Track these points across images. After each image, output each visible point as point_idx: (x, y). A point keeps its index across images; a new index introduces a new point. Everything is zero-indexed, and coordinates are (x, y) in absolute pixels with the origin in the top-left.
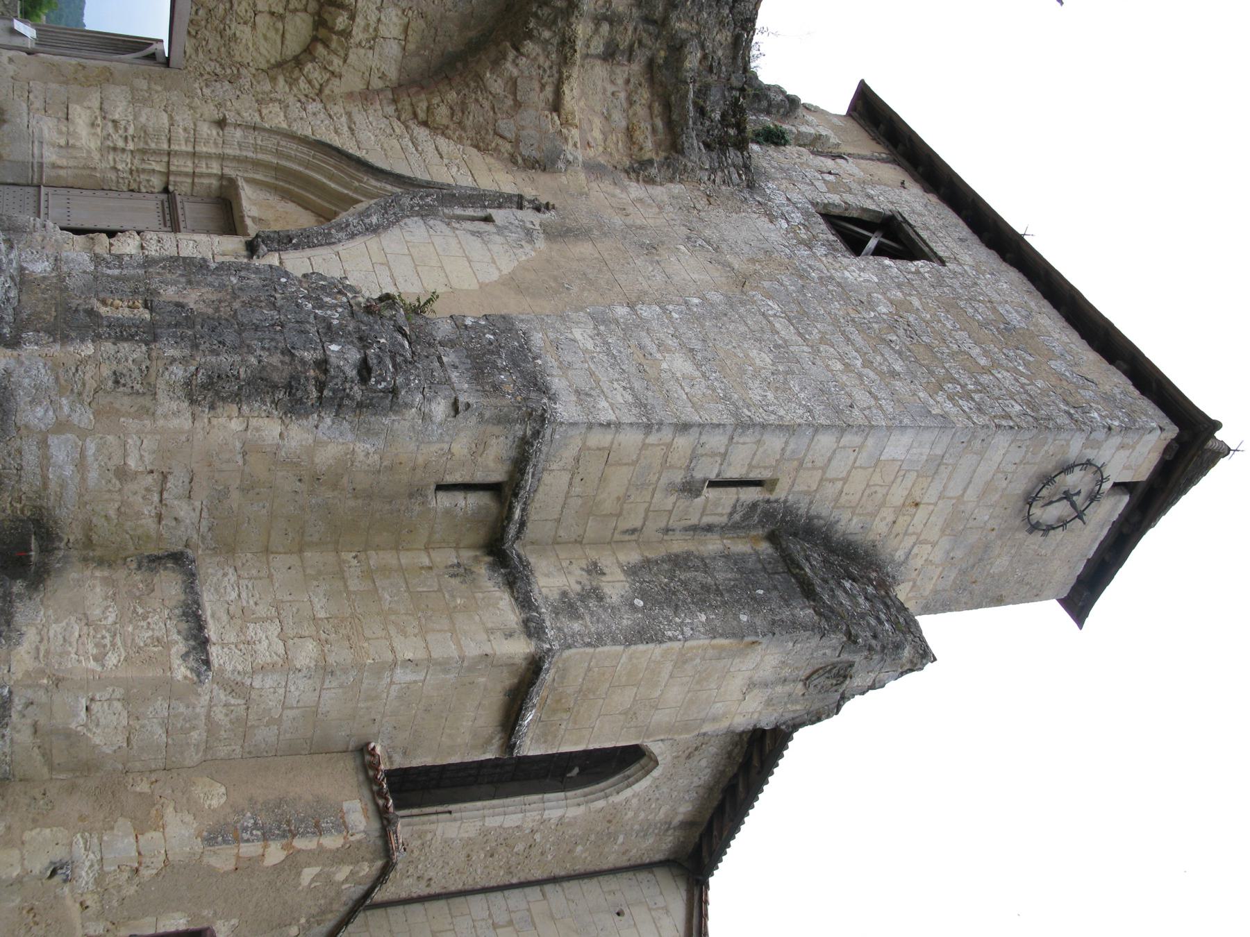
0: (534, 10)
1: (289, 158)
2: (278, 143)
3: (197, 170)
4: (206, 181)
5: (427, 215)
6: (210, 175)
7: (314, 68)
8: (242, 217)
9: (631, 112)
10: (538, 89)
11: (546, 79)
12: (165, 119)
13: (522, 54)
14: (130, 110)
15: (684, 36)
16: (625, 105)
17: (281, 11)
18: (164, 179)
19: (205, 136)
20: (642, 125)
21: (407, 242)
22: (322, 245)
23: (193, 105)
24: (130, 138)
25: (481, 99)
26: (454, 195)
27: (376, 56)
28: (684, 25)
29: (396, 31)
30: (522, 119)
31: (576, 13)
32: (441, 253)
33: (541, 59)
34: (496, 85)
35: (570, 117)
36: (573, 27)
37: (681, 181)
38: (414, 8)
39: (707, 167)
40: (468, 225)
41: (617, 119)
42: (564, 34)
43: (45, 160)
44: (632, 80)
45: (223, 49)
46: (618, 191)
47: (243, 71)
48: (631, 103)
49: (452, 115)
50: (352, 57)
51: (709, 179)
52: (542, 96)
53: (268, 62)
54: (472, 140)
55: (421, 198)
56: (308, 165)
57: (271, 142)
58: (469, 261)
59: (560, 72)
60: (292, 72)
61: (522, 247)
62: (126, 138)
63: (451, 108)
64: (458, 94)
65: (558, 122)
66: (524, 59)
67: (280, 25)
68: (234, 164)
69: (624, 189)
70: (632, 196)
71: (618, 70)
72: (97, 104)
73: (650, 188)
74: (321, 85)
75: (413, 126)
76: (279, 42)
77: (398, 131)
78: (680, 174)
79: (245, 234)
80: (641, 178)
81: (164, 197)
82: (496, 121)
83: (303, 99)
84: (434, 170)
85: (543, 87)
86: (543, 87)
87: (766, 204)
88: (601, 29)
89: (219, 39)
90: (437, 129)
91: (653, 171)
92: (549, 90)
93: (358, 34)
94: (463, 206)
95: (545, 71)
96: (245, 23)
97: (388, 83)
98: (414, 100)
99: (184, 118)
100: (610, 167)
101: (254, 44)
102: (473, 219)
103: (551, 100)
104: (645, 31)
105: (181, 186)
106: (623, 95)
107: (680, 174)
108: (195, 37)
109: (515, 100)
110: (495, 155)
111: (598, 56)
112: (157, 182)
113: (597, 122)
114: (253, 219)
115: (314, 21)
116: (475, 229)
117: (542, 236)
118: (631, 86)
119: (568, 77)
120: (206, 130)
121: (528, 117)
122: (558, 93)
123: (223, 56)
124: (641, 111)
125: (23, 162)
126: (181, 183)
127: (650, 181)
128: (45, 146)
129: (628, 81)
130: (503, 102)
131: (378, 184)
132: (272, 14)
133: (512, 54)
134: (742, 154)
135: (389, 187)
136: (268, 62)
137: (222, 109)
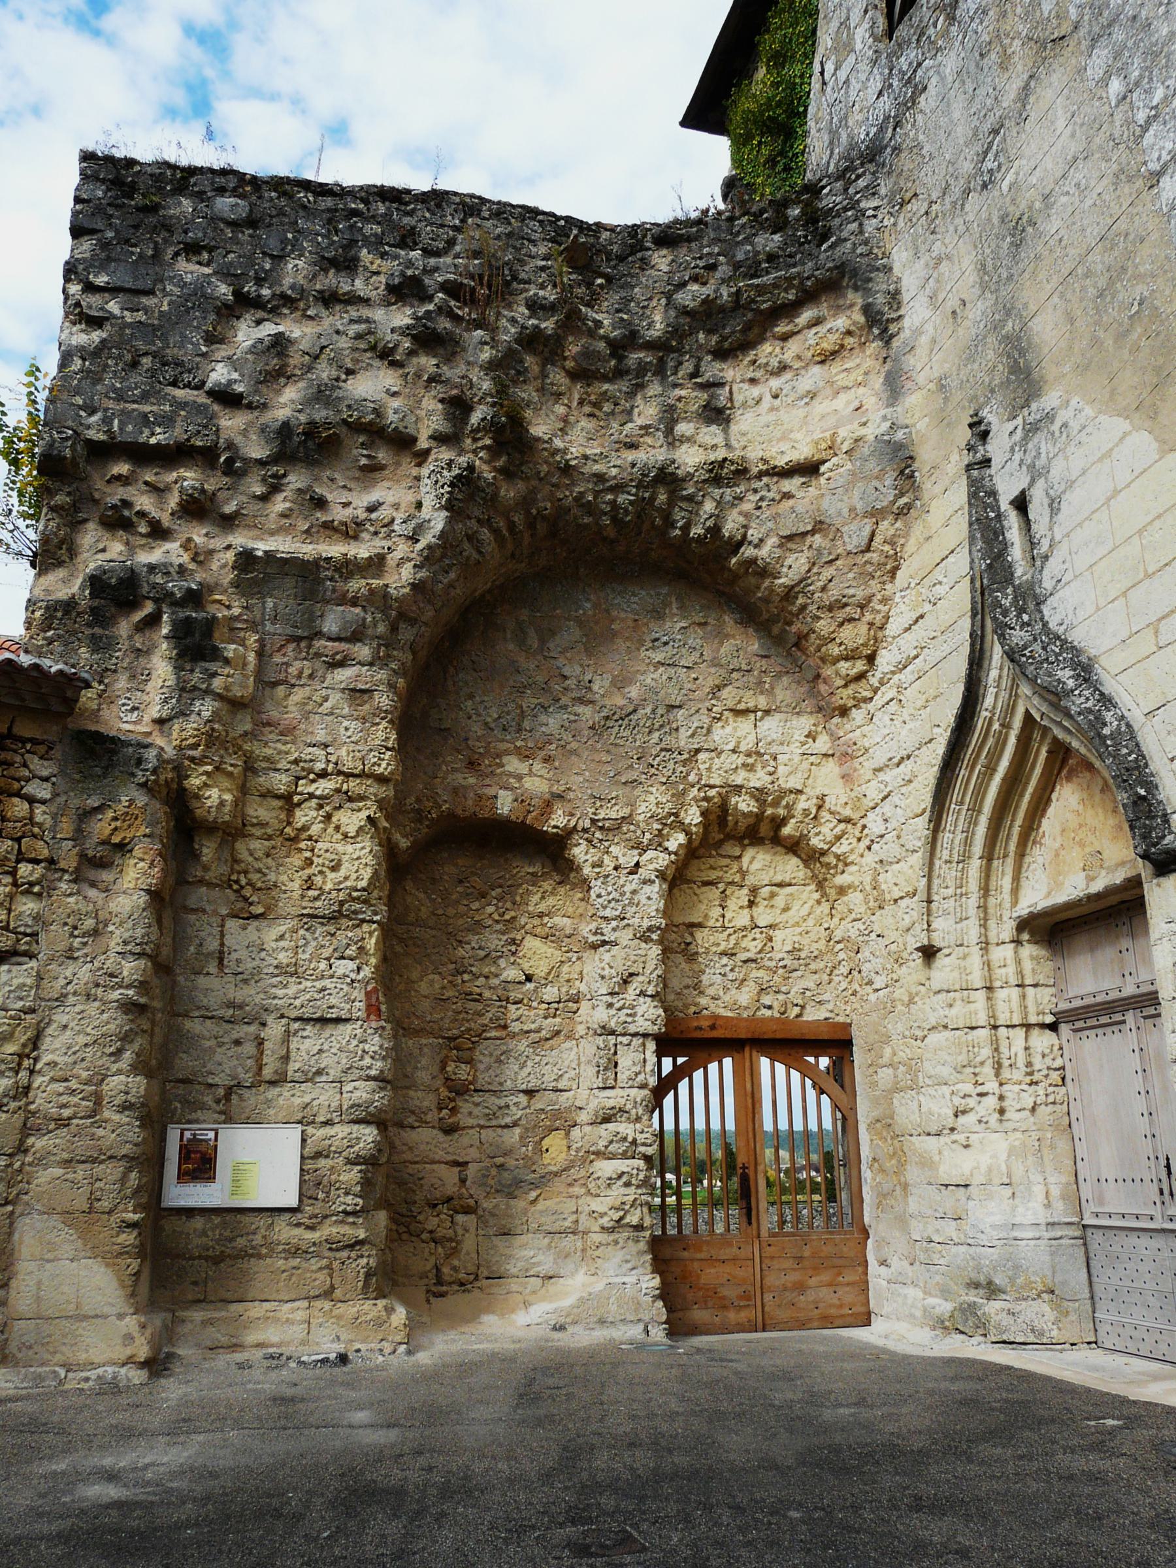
0: (678, 532)
1: (968, 842)
2: (946, 862)
3: (1013, 980)
4: (1028, 965)
5: (1035, 596)
6: (1018, 962)
7: (818, 834)
8: (1090, 898)
9: (797, 365)
10: (791, 502)
11: (771, 495)
12: (934, 1038)
13: (745, 536)
14: (931, 1091)
15: (672, 313)
16: (788, 375)
17: (745, 891)
18: (1036, 1032)
19: (956, 974)
20: (812, 342)
21: (1098, 609)
22: (1137, 745)
23: (906, 999)
24: (980, 1089)
25: (821, 583)
26: (990, 566)
27: (785, 749)
28: (658, 318)
29: (744, 725)
30: (839, 514)
31: (671, 469)
32: (1110, 546)
33: (747, 506)
34: (795, 565)
35: (824, 446)
36: (691, 470)
37: (885, 255)
38: (708, 704)
39: (855, 225)
40: (1040, 527)
41: (811, 382)
42: (704, 481)
43: (1043, 1221)
44: (750, 375)
45: (813, 966)
46: (924, 340)
47: (838, 935)
48: (783, 368)
49: (851, 620)
50: (794, 783)
51: (875, 216)
52: (799, 494)
53: (819, 902)
54: (884, 583)
55: (1005, 613)
56: (976, 809)
57: (946, 873)
58: (1116, 492)
59: (760, 475)
60: (828, 866)
61: (1065, 425)
62: (980, 1095)
63: (841, 624)
64: (819, 618)
65: (834, 460)
66: (750, 532)
67: (765, 892)
68: (992, 924)
69: (918, 332)
70: (927, 313)
71: (738, 398)
72: (932, 1140)
73: (905, 297)
74: (840, 821)
75: (878, 675)
76: (788, 890)
77: (892, 693)
78: (877, 258)
79: (1135, 883)
80: (894, 315)
81: (1064, 1029)
82: (849, 553)
83: (867, 842)
84: (946, 619)
85: (787, 496)
86: (787, 496)
87: (895, 117)
88: (688, 434)
89: (799, 973)
90: (876, 640)
91: (880, 299)
92: (789, 485)
93: (759, 779)
94: (1005, 546)
95: (762, 499)
96: (771, 940)
97: (820, 729)
98: (840, 682)
99: (931, 1010)
100: (887, 367)
101: (797, 924)
102: (1027, 523)
103: (803, 480)
104: (675, 373)
105: (1042, 1004)
106: (775, 383)
107: (877, 258)
108: (803, 1007)
109: (813, 532)
110: (902, 541)
111: (726, 431)
112: (1043, 1041)
113: (821, 406)
114: (1090, 879)
115: (752, 844)
116: (1047, 511)
117: (1034, 406)
118: (758, 374)
119: (764, 460)
120: (944, 970)
121: (834, 507)
122: (787, 472)
123: (822, 965)
124: (794, 347)
125: (1052, 1254)
126: (1038, 1004)
127: (895, 297)
128: (1017, 1220)
129: (753, 381)
130: (818, 550)
131: (992, 691)
132: (751, 904)
133: (748, 552)
134: (824, 187)
135: (994, 674)
136: (819, 902)
137: (905, 955)
